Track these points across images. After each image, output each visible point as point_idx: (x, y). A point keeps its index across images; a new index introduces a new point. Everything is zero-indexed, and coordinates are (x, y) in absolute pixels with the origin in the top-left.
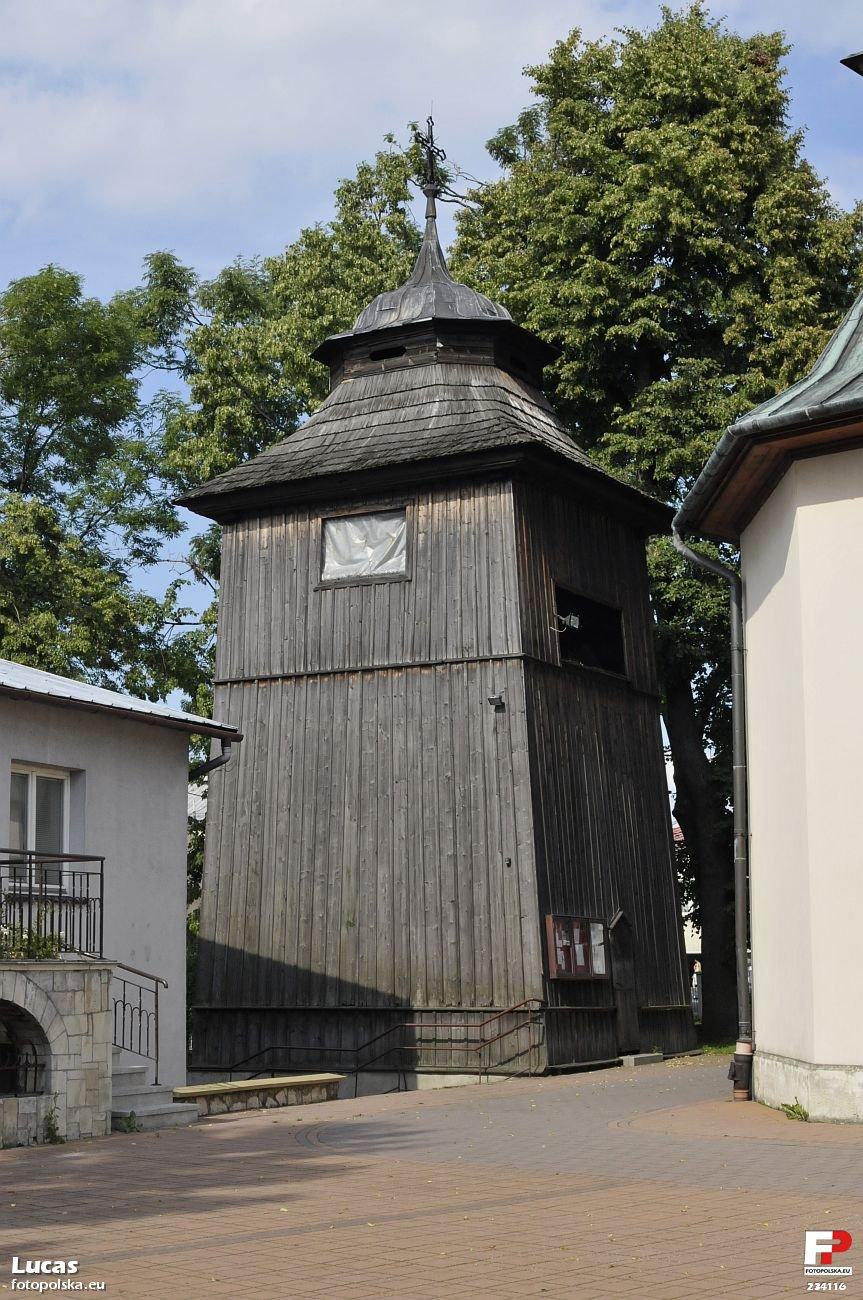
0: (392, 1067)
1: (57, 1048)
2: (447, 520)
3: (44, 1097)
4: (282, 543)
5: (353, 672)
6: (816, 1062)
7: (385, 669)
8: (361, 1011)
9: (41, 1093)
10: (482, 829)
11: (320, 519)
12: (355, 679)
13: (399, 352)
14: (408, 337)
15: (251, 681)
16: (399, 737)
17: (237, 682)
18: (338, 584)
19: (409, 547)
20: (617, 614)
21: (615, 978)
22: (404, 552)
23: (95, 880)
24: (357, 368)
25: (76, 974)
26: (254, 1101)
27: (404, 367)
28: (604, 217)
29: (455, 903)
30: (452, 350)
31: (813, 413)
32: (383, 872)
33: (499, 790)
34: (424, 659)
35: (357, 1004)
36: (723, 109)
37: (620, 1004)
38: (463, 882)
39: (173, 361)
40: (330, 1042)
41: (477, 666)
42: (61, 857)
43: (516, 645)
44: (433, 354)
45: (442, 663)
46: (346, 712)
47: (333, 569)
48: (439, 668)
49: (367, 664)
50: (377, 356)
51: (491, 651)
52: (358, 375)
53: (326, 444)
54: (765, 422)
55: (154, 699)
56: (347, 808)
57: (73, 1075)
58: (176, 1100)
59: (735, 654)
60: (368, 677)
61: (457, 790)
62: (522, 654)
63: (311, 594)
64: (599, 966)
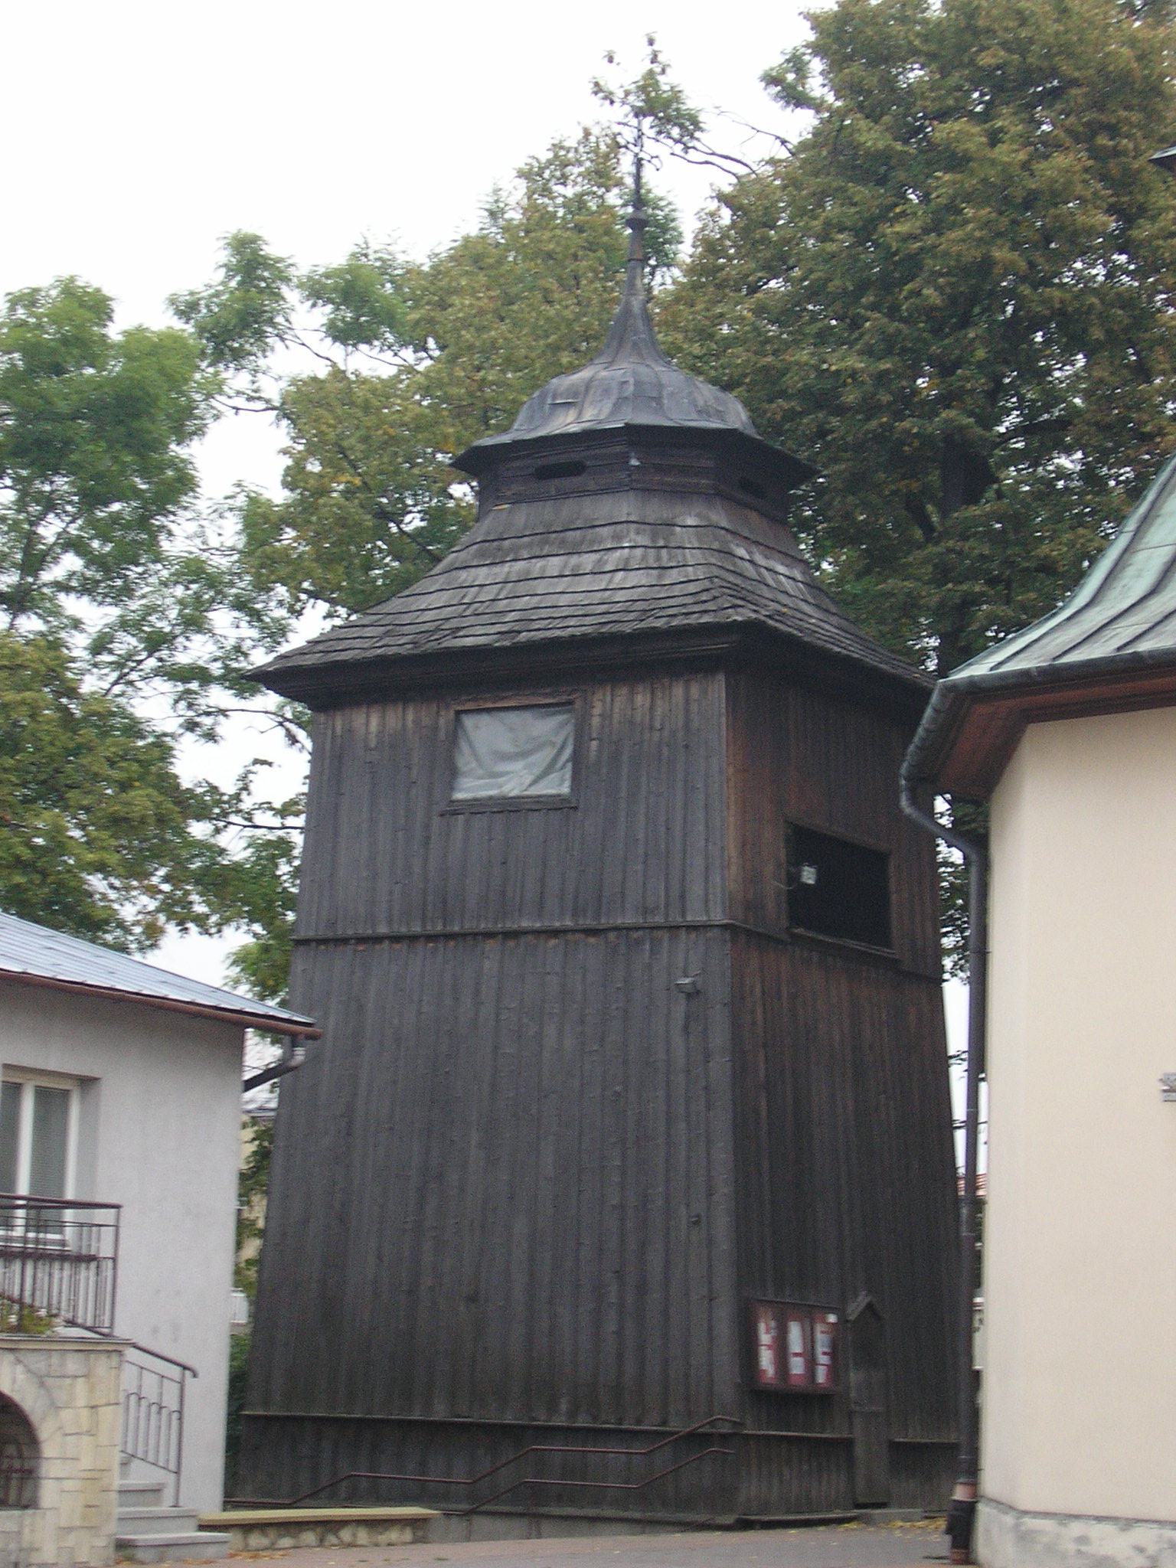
0: (520, 1509)
1: (48, 1450)
2: (632, 723)
3: (30, 1512)
5: (489, 935)
6: (1023, 1507)
7: (537, 933)
8: (478, 1426)
9: (26, 1507)
11: (452, 713)
12: (490, 945)
13: (576, 469)
14: (588, 448)
15: (345, 941)
16: (551, 1030)
17: (324, 941)
18: (477, 807)
19: (577, 759)
20: (882, 858)
22: (570, 765)
23: (108, 1234)
24: (516, 488)
25: (80, 1354)
26: (309, 1537)
27: (583, 493)
28: (895, 254)
29: (619, 1275)
30: (652, 470)
31: (1041, 671)
32: (520, 1227)
34: (589, 922)
36: (1085, 90)
37: (858, 1433)
39: (259, 398)
42: (64, 1202)
43: (719, 910)
44: (623, 475)
45: (616, 929)
46: (477, 992)
47: (468, 789)
48: (612, 936)
49: (511, 925)
50: (546, 473)
51: (683, 914)
52: (517, 500)
53: (465, 601)
54: (983, 677)
55: (334, 626)
57: (69, 1485)
58: (202, 1527)
60: (511, 943)
63: (436, 820)
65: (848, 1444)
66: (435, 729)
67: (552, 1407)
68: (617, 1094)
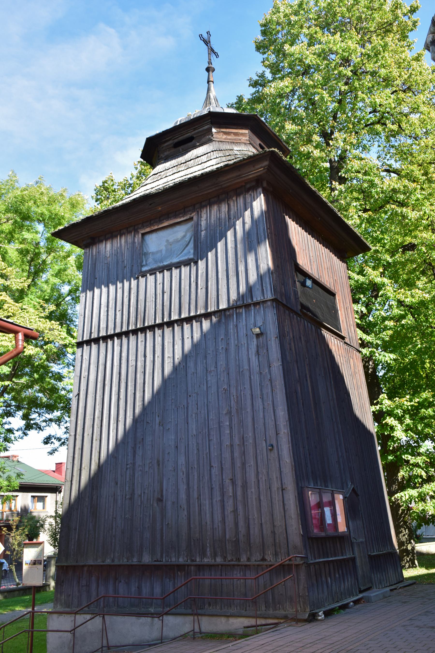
0: (190, 611)
4: (117, 254)
10: (250, 424)
11: (140, 235)
21: (352, 534)
32: (182, 460)
33: (262, 395)
35: (164, 560)
38: (238, 464)
40: (146, 591)
41: (243, 311)
56: (157, 417)
59: (298, 504)
61: (232, 398)
62: (273, 297)
64: (342, 528)
65: (353, 560)
66: (134, 242)
67: (203, 554)
68: (225, 390)
